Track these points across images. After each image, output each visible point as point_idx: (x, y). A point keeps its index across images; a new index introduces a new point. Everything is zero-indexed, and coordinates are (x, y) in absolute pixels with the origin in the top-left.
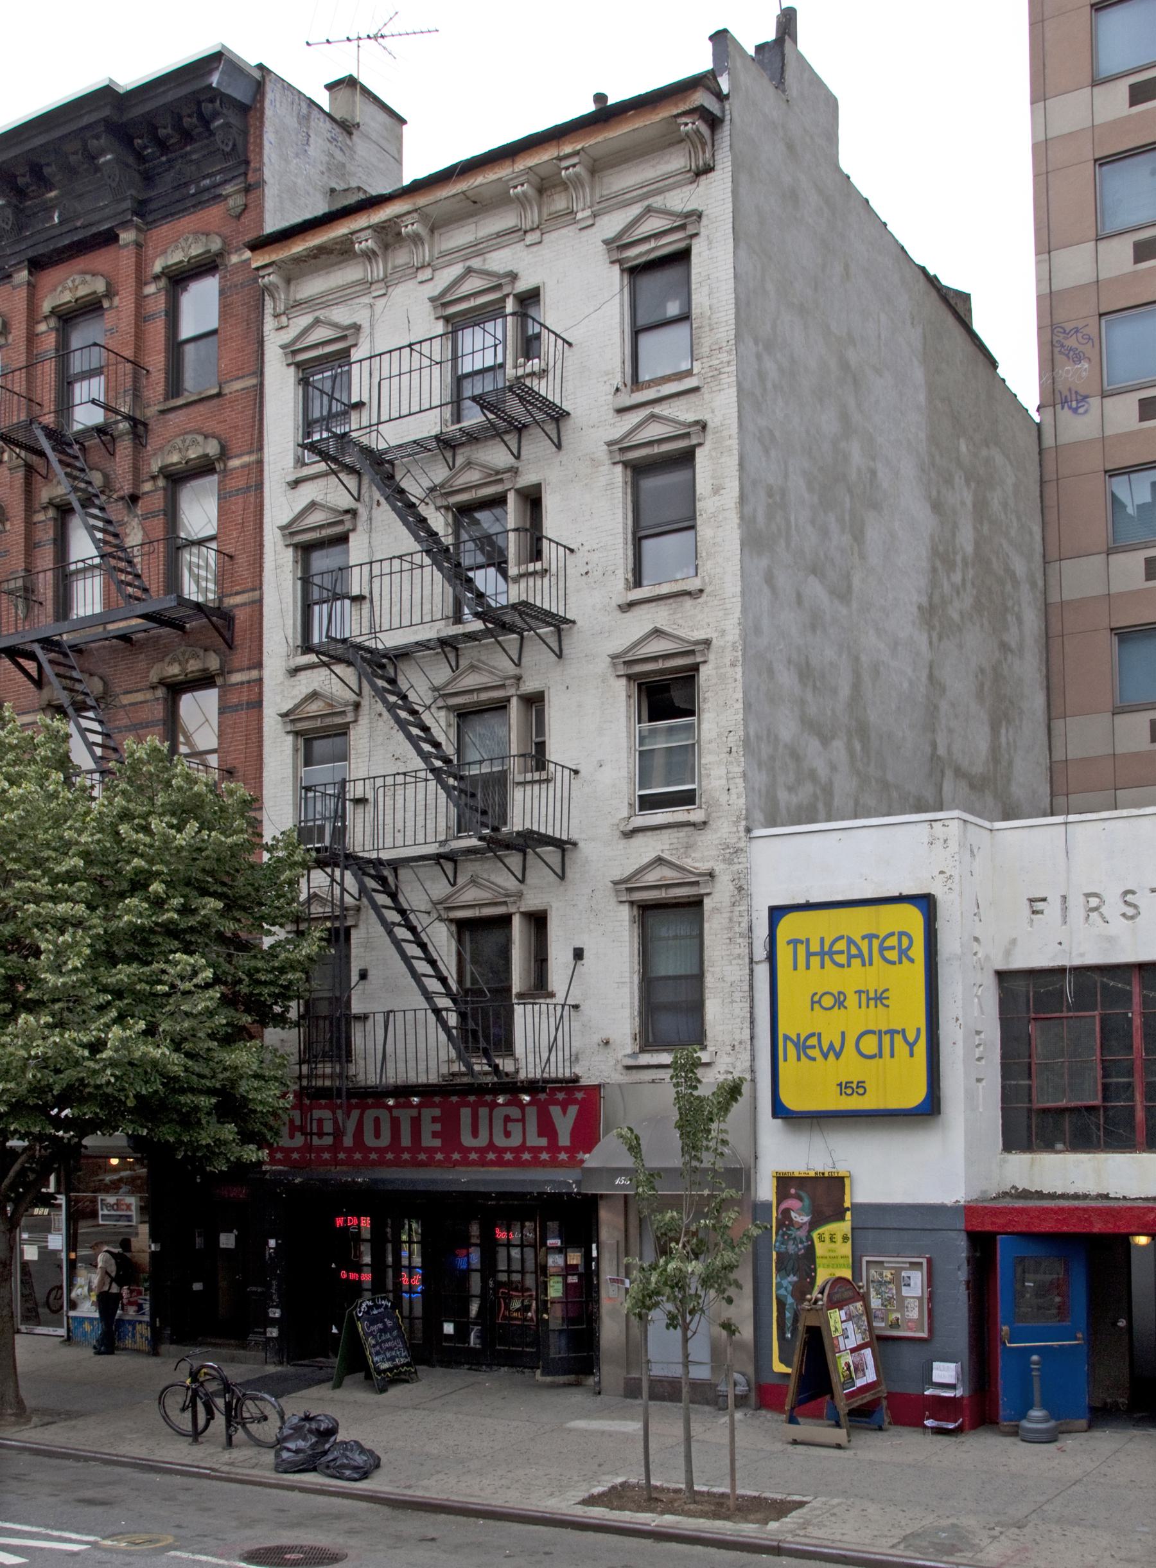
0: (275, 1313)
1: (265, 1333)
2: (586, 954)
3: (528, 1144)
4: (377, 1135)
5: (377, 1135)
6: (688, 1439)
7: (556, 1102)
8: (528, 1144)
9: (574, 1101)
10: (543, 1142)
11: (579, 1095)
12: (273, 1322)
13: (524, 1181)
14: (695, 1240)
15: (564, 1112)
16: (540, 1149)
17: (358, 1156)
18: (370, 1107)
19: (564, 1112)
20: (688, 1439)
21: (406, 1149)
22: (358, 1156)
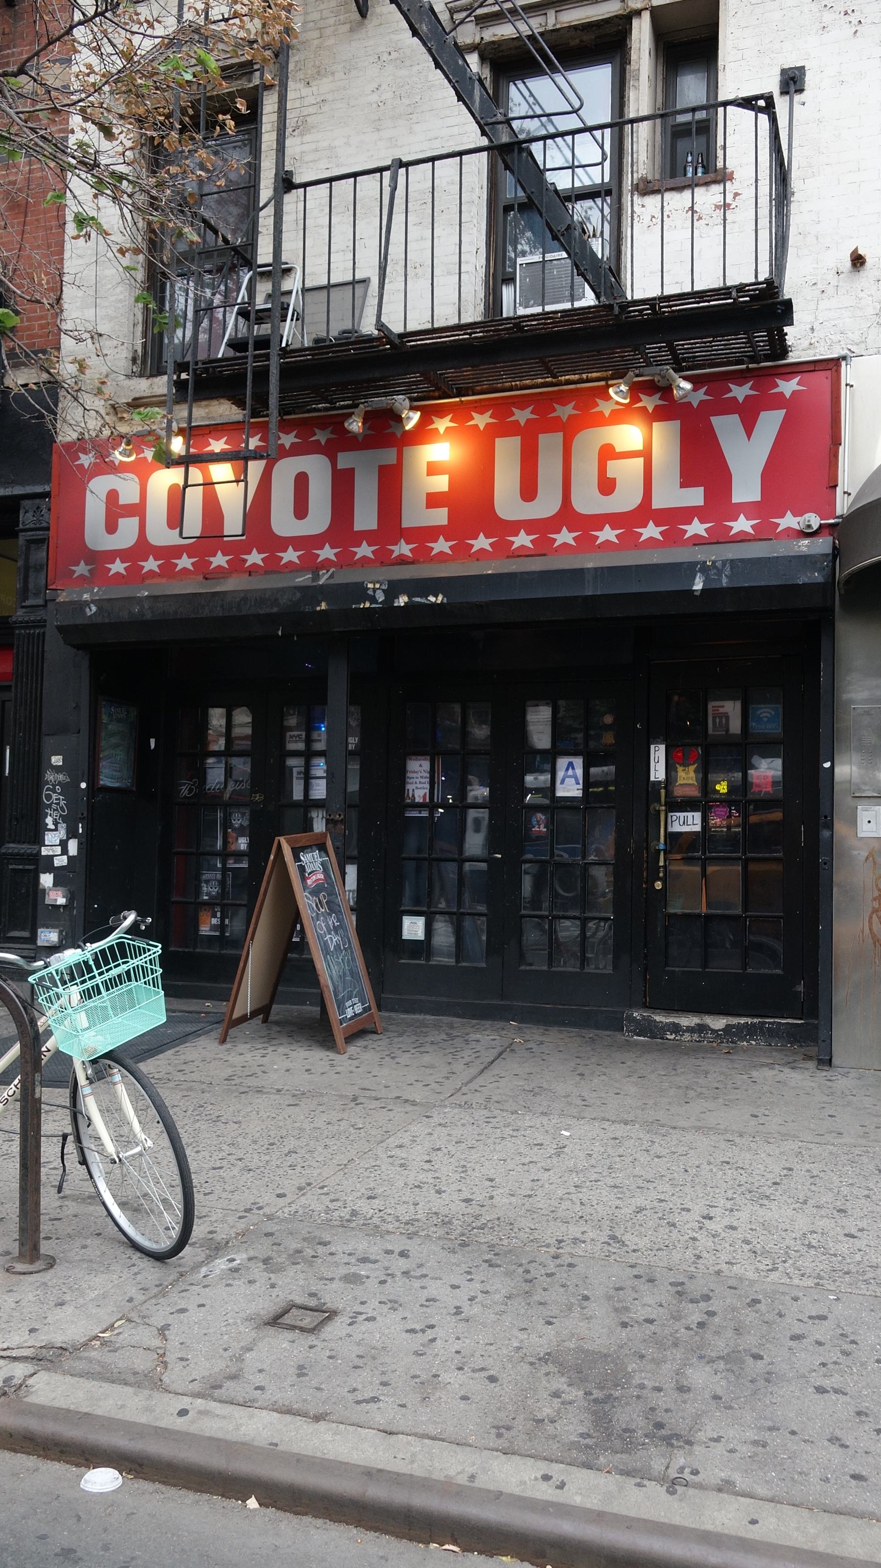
0: (608, 719)
1: (33, 938)
2: (810, 79)
3: (657, 503)
4: (301, 510)
5: (301, 510)
6: (725, 220)
7: (731, 407)
8: (657, 503)
9: (778, 401)
10: (695, 497)
11: (788, 387)
12: (607, 728)
13: (581, 572)
14: (165, 421)
15: (749, 428)
16: (687, 514)
17: (255, 558)
18: (284, 453)
19: (749, 428)
20: (725, 220)
21: (368, 536)
22: (255, 558)
